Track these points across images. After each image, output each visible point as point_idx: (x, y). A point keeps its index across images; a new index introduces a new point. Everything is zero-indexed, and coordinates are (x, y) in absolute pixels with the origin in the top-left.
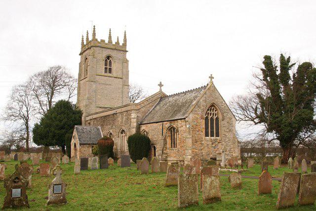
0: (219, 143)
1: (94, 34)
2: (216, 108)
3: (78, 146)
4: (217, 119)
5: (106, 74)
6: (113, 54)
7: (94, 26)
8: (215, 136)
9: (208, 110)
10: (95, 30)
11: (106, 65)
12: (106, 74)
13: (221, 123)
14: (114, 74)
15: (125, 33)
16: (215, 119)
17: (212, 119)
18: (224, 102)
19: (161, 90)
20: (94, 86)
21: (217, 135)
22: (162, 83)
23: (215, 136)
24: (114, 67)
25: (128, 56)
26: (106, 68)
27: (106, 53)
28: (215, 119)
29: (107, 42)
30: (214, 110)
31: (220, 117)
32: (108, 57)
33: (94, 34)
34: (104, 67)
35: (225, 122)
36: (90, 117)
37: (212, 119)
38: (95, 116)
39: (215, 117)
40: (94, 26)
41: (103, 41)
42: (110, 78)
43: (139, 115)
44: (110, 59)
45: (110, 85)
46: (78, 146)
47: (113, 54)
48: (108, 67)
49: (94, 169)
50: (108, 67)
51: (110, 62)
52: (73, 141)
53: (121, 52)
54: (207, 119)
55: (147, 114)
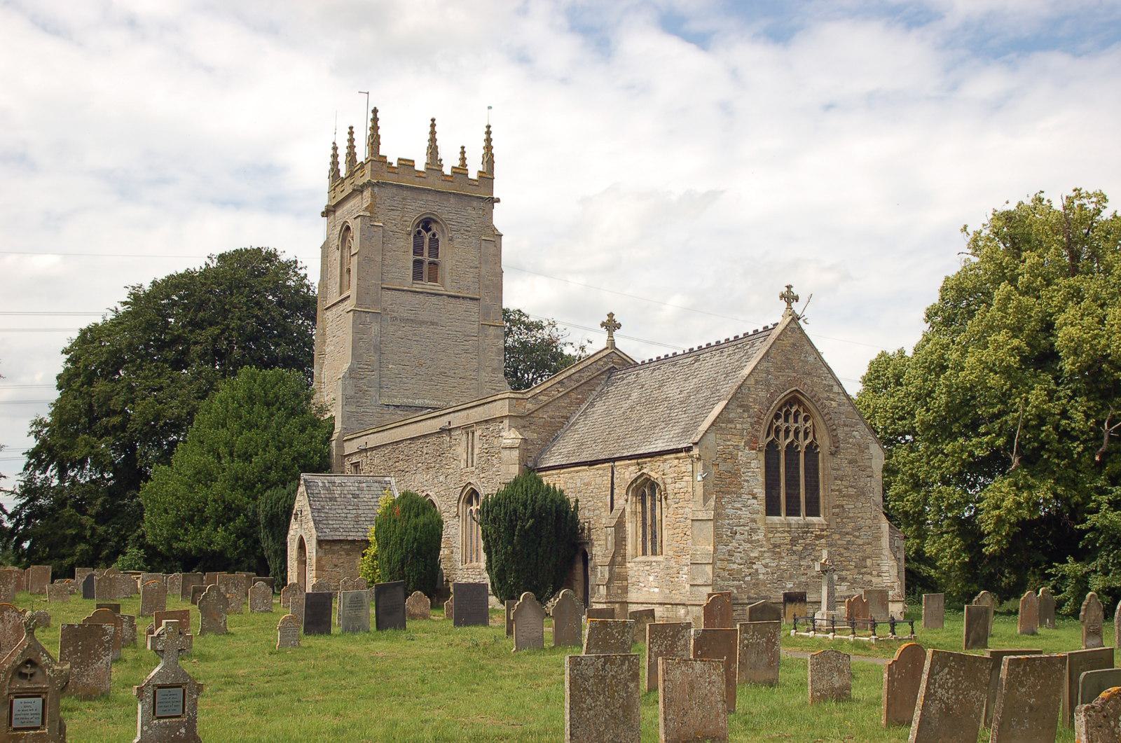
0: (818, 537)
1: (374, 141)
3: (311, 548)
4: (812, 450)
5: (418, 287)
7: (489, 127)
8: (783, 513)
9: (777, 417)
11: (418, 249)
12: (418, 287)
13: (825, 465)
14: (447, 285)
15: (488, 133)
16: (802, 449)
17: (791, 449)
18: (836, 389)
20: (375, 328)
21: (813, 510)
23: (783, 513)
24: (449, 257)
25: (500, 218)
26: (418, 264)
27: (416, 209)
28: (802, 449)
29: (420, 165)
30: (800, 419)
31: (824, 443)
32: (426, 224)
33: (374, 141)
34: (411, 257)
35: (842, 460)
37: (791, 449)
39: (803, 444)
41: (407, 164)
42: (434, 299)
44: (434, 227)
45: (432, 323)
46: (311, 548)
47: (446, 211)
48: (426, 257)
50: (426, 257)
51: (434, 242)
53: (475, 204)
54: (771, 450)
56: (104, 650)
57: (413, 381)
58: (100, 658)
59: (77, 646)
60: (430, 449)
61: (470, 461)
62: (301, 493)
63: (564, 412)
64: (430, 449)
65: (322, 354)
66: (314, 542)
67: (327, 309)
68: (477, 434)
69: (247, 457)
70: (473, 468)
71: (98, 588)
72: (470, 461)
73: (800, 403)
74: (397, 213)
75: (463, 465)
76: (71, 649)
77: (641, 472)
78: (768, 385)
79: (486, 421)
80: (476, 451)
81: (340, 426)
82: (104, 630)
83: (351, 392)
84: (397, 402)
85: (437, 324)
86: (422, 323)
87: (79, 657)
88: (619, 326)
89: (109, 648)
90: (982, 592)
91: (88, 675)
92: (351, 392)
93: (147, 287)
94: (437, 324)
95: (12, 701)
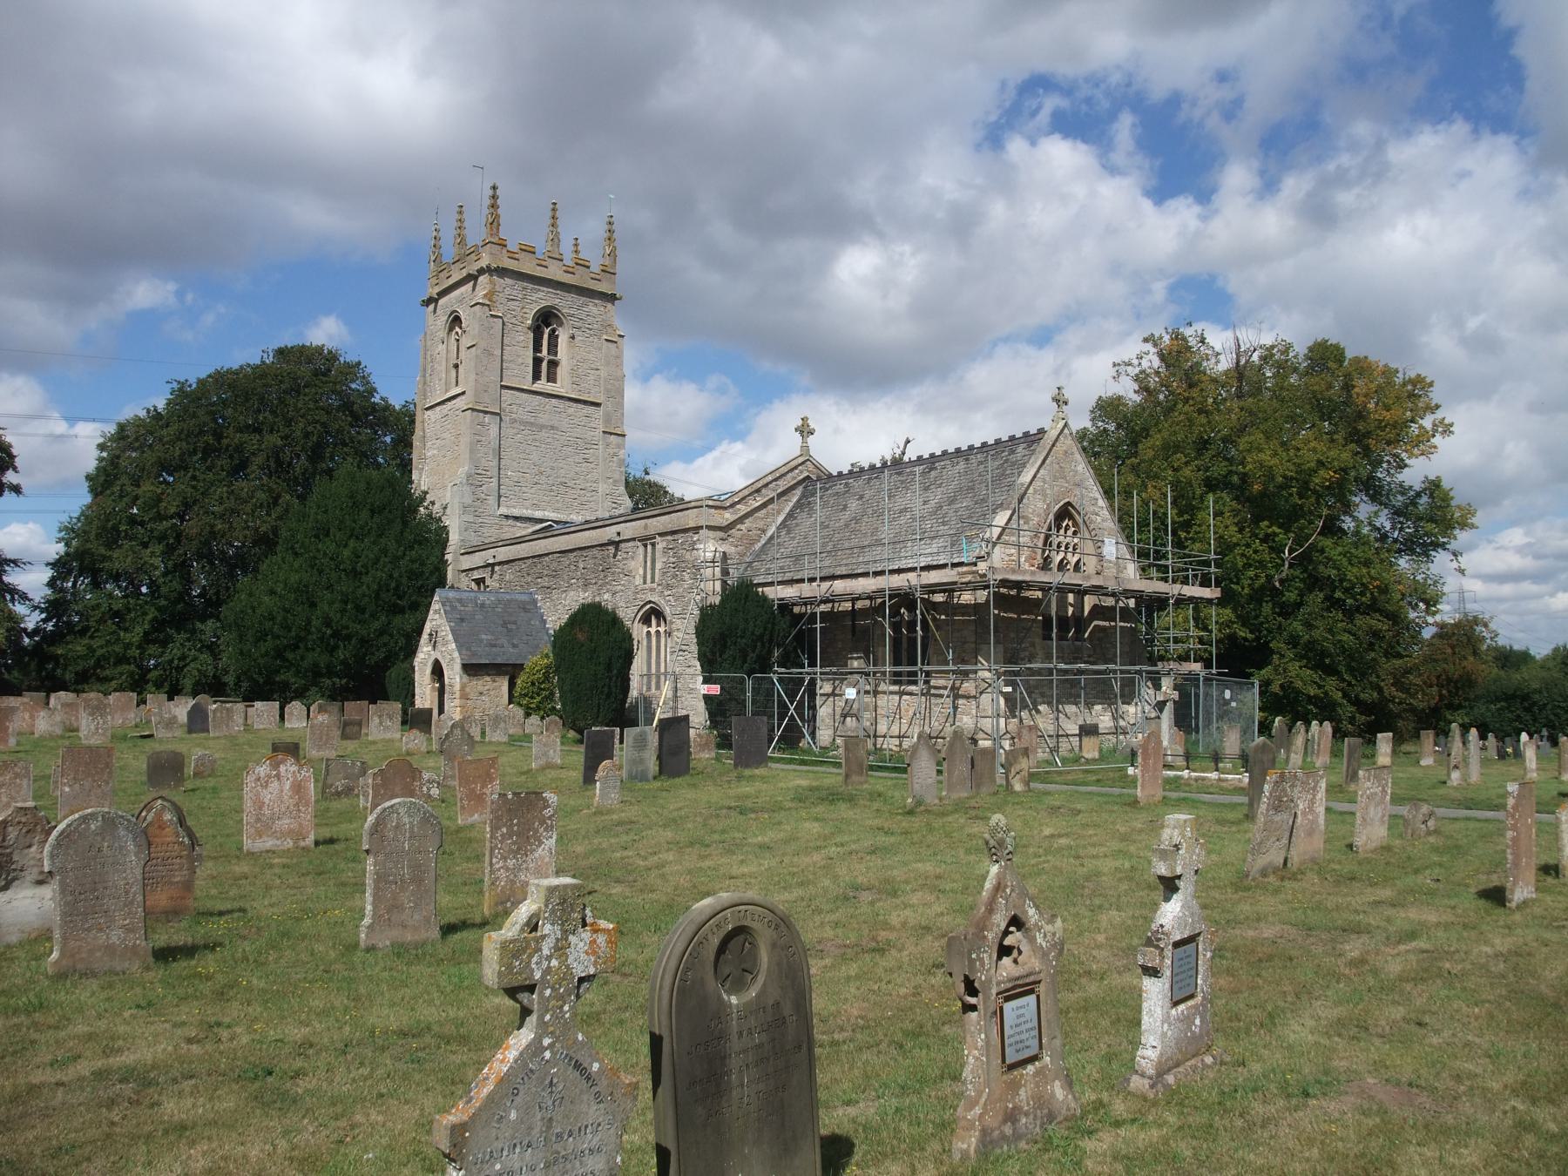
1: (494, 223)
2: (1076, 524)
3: (454, 675)
6: (564, 303)
7: (494, 188)
10: (558, 214)
11: (537, 347)
12: (538, 386)
19: (805, 449)
22: (1067, 394)
26: (537, 362)
27: (542, 298)
30: (1070, 533)
33: (494, 223)
36: (478, 559)
38: (504, 553)
40: (494, 188)
43: (731, 550)
45: (553, 428)
46: (454, 675)
49: (1006, 933)
52: (424, 656)
55: (758, 546)
56: (546, 830)
57: (533, 491)
58: (541, 843)
59: (512, 825)
60: (590, 563)
61: (649, 577)
62: (436, 612)
63: (761, 524)
64: (590, 563)
65: (423, 458)
66: (458, 667)
67: (427, 409)
68: (659, 547)
69: (355, 574)
70: (655, 585)
71: (214, 720)
72: (649, 577)
73: (1071, 517)
74: (517, 303)
75: (638, 581)
76: (504, 830)
77: (1155, 586)
78: (1045, 495)
79: (673, 533)
80: (659, 565)
81: (457, 537)
82: (545, 800)
83: (468, 500)
84: (516, 512)
85: (557, 429)
86: (542, 427)
87: (514, 843)
88: (811, 433)
89: (552, 826)
90: (1277, 719)
91: (527, 869)
92: (468, 500)
93: (193, 381)
94: (557, 429)
95: (1001, 1008)
